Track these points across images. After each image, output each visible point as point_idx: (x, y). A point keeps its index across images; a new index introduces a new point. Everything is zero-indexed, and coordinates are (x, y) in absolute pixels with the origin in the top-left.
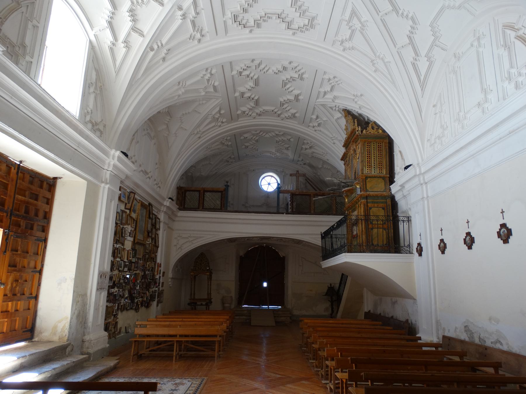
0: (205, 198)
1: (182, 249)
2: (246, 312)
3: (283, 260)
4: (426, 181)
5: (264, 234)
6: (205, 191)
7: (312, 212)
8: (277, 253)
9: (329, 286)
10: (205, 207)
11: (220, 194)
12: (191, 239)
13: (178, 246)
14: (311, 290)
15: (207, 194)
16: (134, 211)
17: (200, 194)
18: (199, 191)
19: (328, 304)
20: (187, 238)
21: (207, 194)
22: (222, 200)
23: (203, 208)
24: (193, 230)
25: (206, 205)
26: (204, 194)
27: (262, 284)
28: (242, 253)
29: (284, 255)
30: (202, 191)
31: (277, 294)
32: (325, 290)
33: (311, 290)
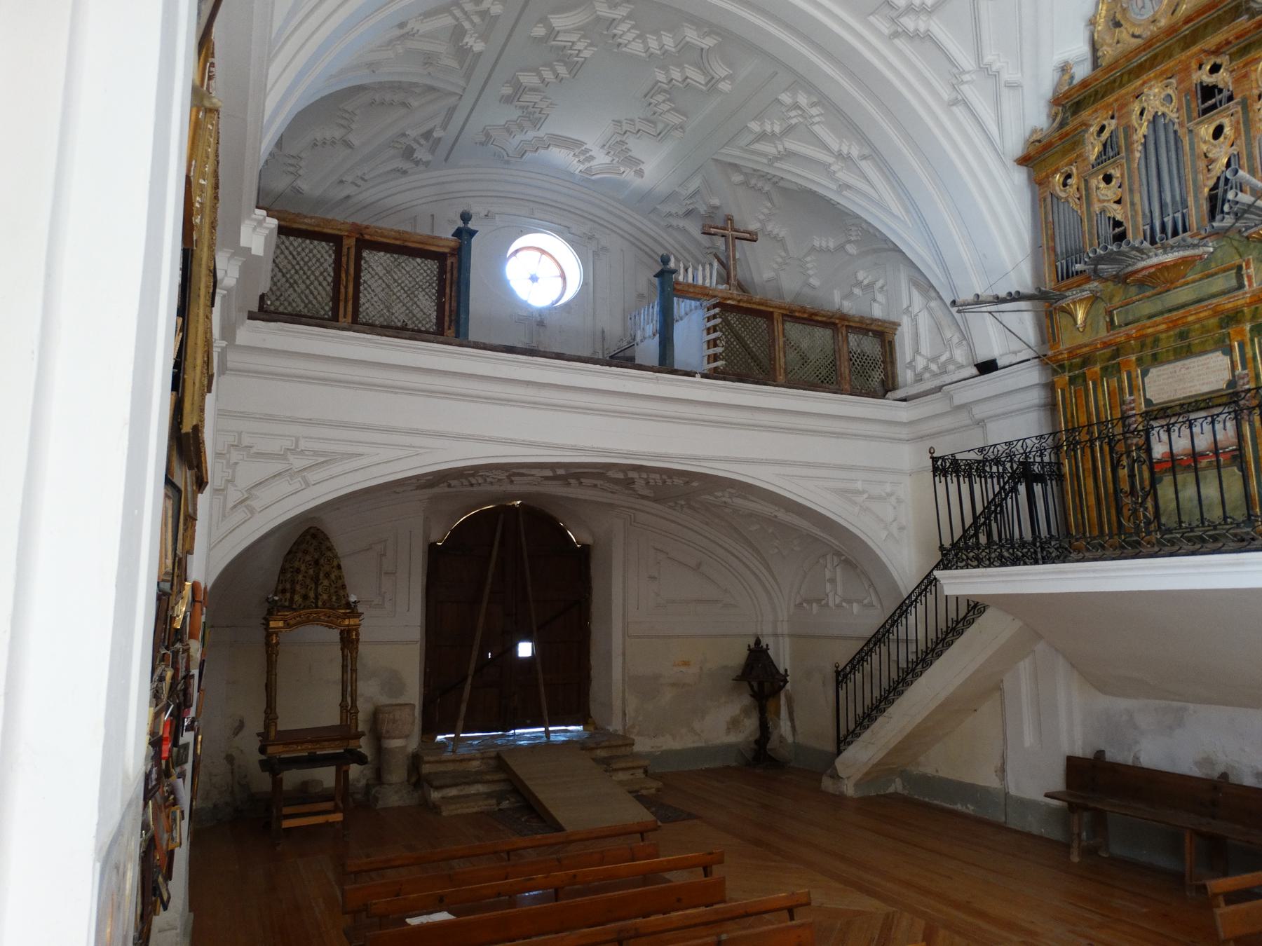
0: (365, 276)
1: (252, 511)
2: (476, 763)
3: (583, 556)
4: (1057, 317)
5: (592, 450)
6: (367, 242)
7: (781, 378)
8: (563, 532)
9: (752, 646)
10: (362, 318)
11: (433, 265)
12: (298, 463)
13: (234, 496)
14: (686, 664)
15: (376, 262)
16: (584, 31)
17: (338, 253)
18: (336, 240)
19: (746, 700)
20: (281, 457)
21: (376, 262)
22: (441, 292)
23: (355, 320)
24: (310, 422)
25: (370, 306)
26: (359, 258)
27: (536, 649)
28: (439, 535)
29: (588, 539)
30: (349, 243)
31: (566, 684)
32: (737, 656)
33: (686, 664)
